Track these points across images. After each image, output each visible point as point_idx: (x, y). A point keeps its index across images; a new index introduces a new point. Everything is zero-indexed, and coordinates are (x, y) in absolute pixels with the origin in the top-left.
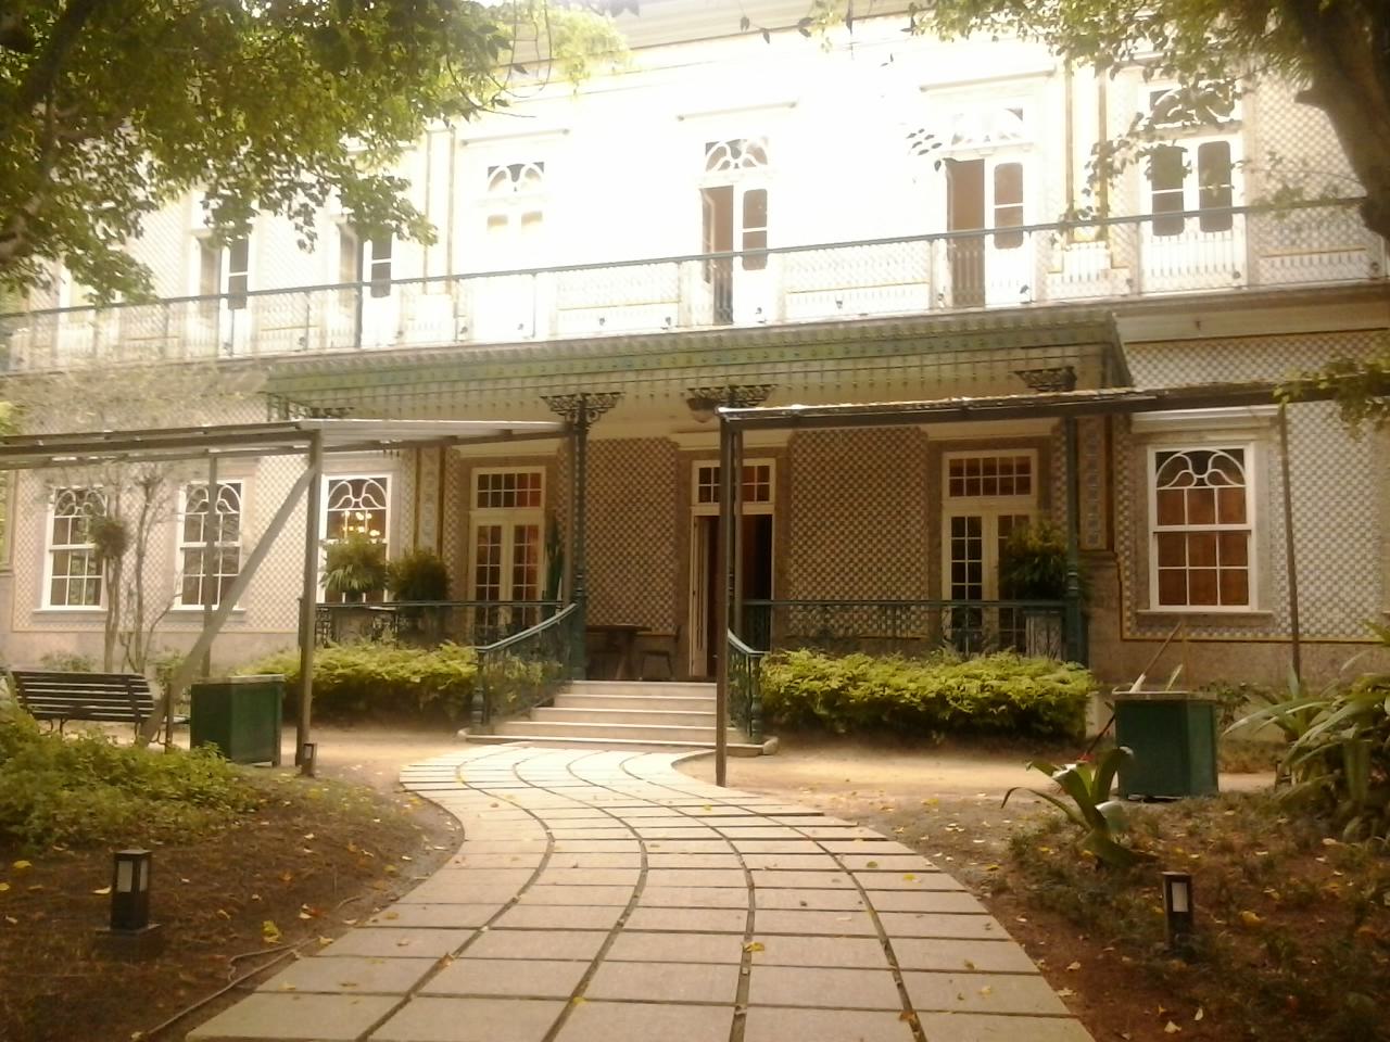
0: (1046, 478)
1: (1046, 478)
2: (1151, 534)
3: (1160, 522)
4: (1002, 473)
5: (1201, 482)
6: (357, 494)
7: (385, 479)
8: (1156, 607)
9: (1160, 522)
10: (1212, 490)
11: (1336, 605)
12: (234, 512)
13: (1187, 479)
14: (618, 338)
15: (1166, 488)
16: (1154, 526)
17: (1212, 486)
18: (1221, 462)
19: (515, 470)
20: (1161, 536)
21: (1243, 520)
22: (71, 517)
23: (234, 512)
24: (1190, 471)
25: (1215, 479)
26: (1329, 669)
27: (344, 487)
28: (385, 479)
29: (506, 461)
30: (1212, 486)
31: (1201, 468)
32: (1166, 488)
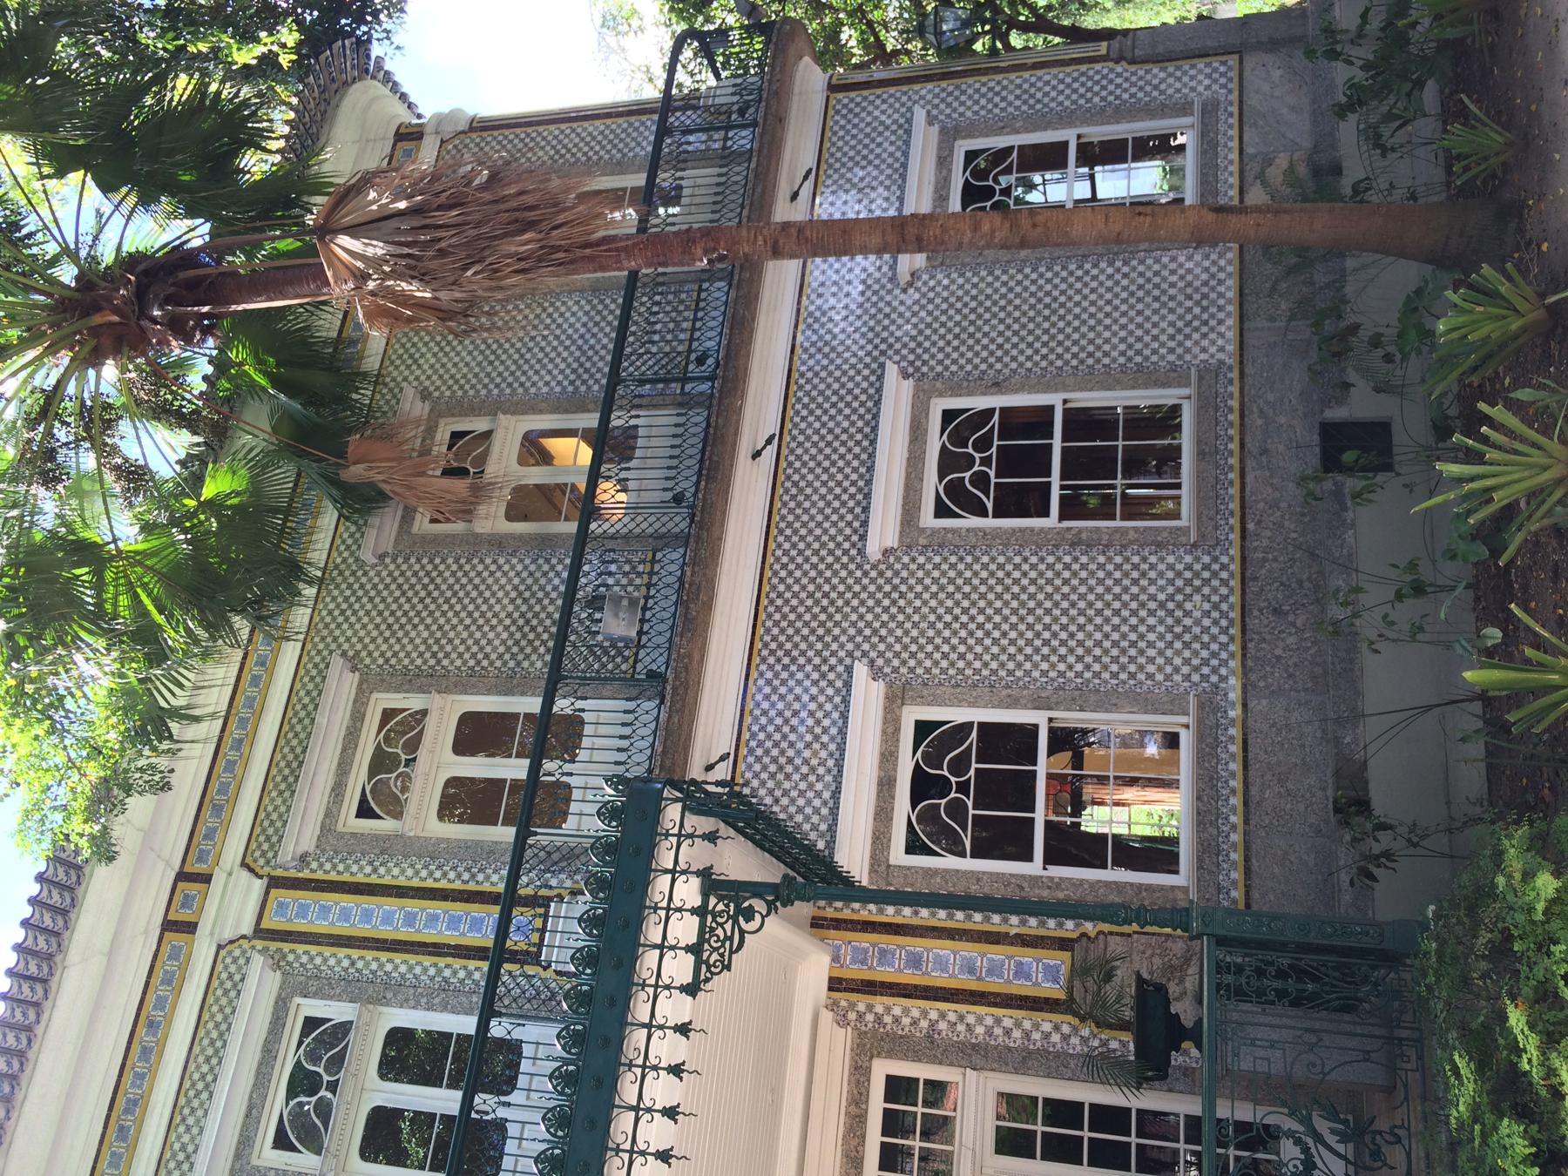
0: (930, 1047)
1: (930, 1047)
2: (1045, 873)
3: (1028, 857)
4: (908, 1152)
5: (963, 788)
6: (942, 786)
7: (938, 515)
8: (1182, 878)
9: (1028, 857)
10: (977, 770)
11: (1179, 606)
12: (1015, 154)
13: (957, 810)
14: (743, 396)
15: (990, 506)
16: (1035, 867)
17: (972, 772)
18: (958, 438)
19: (874, 1137)
20: (1050, 859)
21: (1051, 408)
22: (993, 480)
23: (1015, 154)
24: (967, 475)
25: (959, 766)
26: (1291, 618)
27: (949, 489)
28: (938, 515)
29: (856, 1121)
30: (972, 772)
31: (942, 786)
32: (990, 506)
